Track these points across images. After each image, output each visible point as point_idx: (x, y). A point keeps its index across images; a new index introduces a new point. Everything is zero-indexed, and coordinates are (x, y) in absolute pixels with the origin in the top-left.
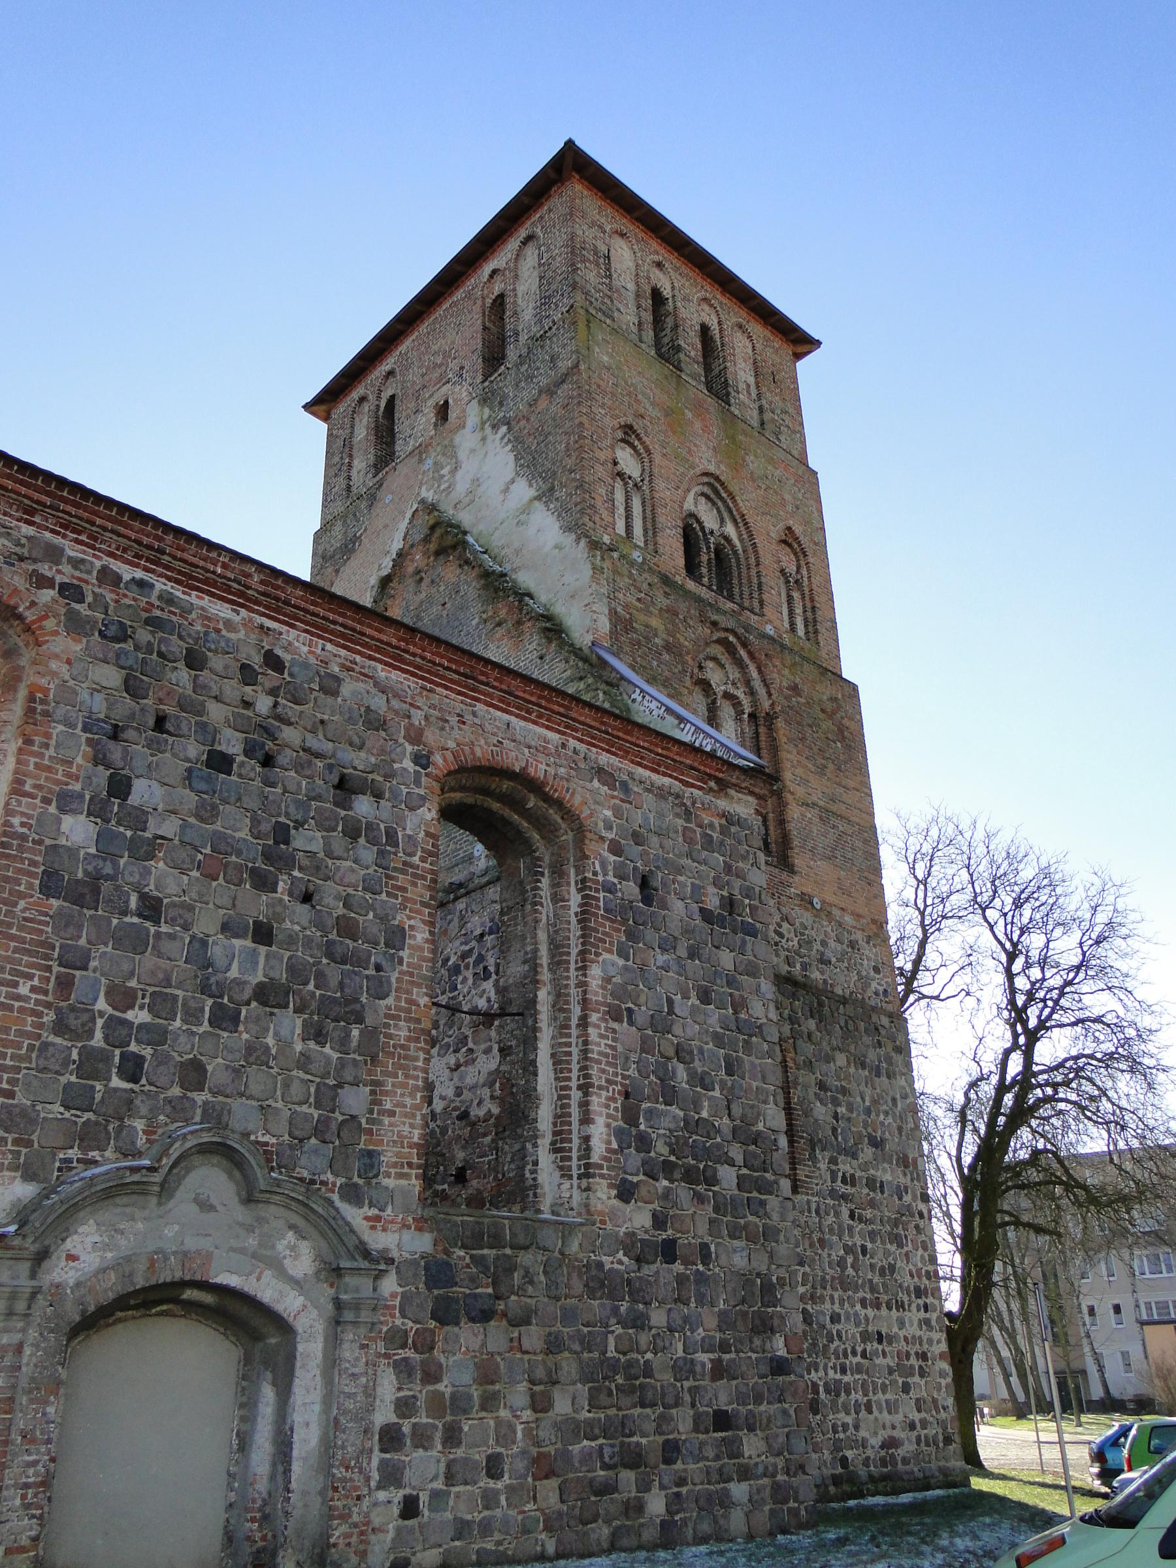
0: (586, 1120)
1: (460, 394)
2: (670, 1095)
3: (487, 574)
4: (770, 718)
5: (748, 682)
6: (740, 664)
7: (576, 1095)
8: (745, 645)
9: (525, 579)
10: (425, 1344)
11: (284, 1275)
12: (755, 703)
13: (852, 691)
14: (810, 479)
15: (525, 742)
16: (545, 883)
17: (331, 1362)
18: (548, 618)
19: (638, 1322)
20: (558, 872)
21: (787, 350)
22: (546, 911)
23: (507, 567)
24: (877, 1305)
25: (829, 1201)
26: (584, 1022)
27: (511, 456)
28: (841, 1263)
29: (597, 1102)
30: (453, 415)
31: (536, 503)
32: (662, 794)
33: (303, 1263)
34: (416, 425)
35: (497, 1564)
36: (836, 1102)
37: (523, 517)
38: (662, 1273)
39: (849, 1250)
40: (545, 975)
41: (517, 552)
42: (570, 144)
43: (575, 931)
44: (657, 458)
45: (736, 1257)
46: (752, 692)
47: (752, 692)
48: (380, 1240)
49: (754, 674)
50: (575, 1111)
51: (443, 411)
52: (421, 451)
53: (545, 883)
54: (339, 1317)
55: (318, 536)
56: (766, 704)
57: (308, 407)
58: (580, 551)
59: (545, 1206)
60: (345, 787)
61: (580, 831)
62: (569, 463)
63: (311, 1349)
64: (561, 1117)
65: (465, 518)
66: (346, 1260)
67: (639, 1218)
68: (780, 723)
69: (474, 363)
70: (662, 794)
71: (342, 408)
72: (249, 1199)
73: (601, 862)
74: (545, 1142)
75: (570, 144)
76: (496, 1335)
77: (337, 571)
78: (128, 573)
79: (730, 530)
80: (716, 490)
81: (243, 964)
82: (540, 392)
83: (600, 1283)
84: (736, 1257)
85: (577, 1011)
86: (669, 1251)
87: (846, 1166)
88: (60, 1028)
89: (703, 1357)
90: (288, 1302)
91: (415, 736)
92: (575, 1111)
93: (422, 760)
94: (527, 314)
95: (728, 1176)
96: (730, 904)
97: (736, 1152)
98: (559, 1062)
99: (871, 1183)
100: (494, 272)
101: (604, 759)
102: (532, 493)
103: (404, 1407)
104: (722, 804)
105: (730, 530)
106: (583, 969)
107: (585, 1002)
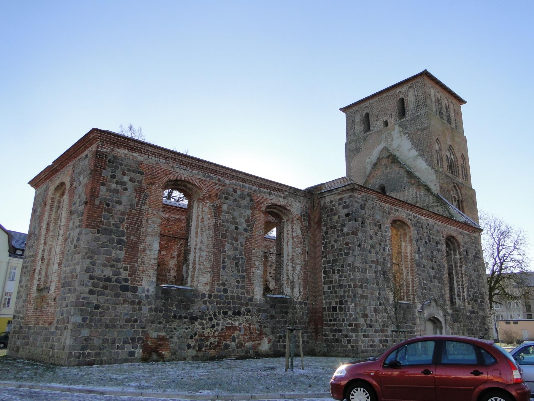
0: (463, 292)
2: (472, 288)
3: (408, 172)
4: (462, 202)
5: (457, 194)
6: (457, 190)
7: (461, 288)
8: (458, 186)
9: (417, 174)
10: (452, 325)
12: (459, 198)
14: (465, 139)
16: (452, 252)
17: (446, 327)
18: (426, 186)
19: (471, 323)
20: (455, 251)
21: (458, 103)
22: (453, 257)
23: (412, 170)
26: (462, 277)
27: (410, 143)
29: (465, 289)
30: (389, 125)
31: (419, 157)
32: (467, 235)
33: (442, 315)
34: (377, 125)
37: (415, 159)
38: (473, 315)
40: (454, 268)
41: (415, 167)
42: (426, 70)
43: (459, 261)
44: (442, 145)
46: (458, 196)
47: (458, 196)
49: (459, 191)
50: (461, 291)
51: (386, 123)
52: (380, 132)
53: (452, 252)
55: (346, 144)
56: (461, 198)
57: (340, 109)
58: (433, 171)
59: (457, 305)
61: (459, 244)
62: (428, 150)
64: (459, 291)
65: (397, 154)
67: (470, 308)
68: (464, 203)
69: (396, 113)
71: (350, 111)
72: (437, 306)
74: (456, 295)
75: (426, 70)
77: (355, 155)
78: (415, 215)
80: (450, 148)
82: (418, 129)
83: (468, 317)
85: (460, 275)
86: (474, 312)
89: (478, 328)
91: (442, 233)
92: (461, 291)
93: (443, 237)
94: (411, 107)
95: (479, 300)
98: (458, 283)
100: (400, 92)
101: (461, 230)
102: (417, 153)
104: (474, 235)
105: (452, 156)
106: (461, 268)
107: (462, 273)
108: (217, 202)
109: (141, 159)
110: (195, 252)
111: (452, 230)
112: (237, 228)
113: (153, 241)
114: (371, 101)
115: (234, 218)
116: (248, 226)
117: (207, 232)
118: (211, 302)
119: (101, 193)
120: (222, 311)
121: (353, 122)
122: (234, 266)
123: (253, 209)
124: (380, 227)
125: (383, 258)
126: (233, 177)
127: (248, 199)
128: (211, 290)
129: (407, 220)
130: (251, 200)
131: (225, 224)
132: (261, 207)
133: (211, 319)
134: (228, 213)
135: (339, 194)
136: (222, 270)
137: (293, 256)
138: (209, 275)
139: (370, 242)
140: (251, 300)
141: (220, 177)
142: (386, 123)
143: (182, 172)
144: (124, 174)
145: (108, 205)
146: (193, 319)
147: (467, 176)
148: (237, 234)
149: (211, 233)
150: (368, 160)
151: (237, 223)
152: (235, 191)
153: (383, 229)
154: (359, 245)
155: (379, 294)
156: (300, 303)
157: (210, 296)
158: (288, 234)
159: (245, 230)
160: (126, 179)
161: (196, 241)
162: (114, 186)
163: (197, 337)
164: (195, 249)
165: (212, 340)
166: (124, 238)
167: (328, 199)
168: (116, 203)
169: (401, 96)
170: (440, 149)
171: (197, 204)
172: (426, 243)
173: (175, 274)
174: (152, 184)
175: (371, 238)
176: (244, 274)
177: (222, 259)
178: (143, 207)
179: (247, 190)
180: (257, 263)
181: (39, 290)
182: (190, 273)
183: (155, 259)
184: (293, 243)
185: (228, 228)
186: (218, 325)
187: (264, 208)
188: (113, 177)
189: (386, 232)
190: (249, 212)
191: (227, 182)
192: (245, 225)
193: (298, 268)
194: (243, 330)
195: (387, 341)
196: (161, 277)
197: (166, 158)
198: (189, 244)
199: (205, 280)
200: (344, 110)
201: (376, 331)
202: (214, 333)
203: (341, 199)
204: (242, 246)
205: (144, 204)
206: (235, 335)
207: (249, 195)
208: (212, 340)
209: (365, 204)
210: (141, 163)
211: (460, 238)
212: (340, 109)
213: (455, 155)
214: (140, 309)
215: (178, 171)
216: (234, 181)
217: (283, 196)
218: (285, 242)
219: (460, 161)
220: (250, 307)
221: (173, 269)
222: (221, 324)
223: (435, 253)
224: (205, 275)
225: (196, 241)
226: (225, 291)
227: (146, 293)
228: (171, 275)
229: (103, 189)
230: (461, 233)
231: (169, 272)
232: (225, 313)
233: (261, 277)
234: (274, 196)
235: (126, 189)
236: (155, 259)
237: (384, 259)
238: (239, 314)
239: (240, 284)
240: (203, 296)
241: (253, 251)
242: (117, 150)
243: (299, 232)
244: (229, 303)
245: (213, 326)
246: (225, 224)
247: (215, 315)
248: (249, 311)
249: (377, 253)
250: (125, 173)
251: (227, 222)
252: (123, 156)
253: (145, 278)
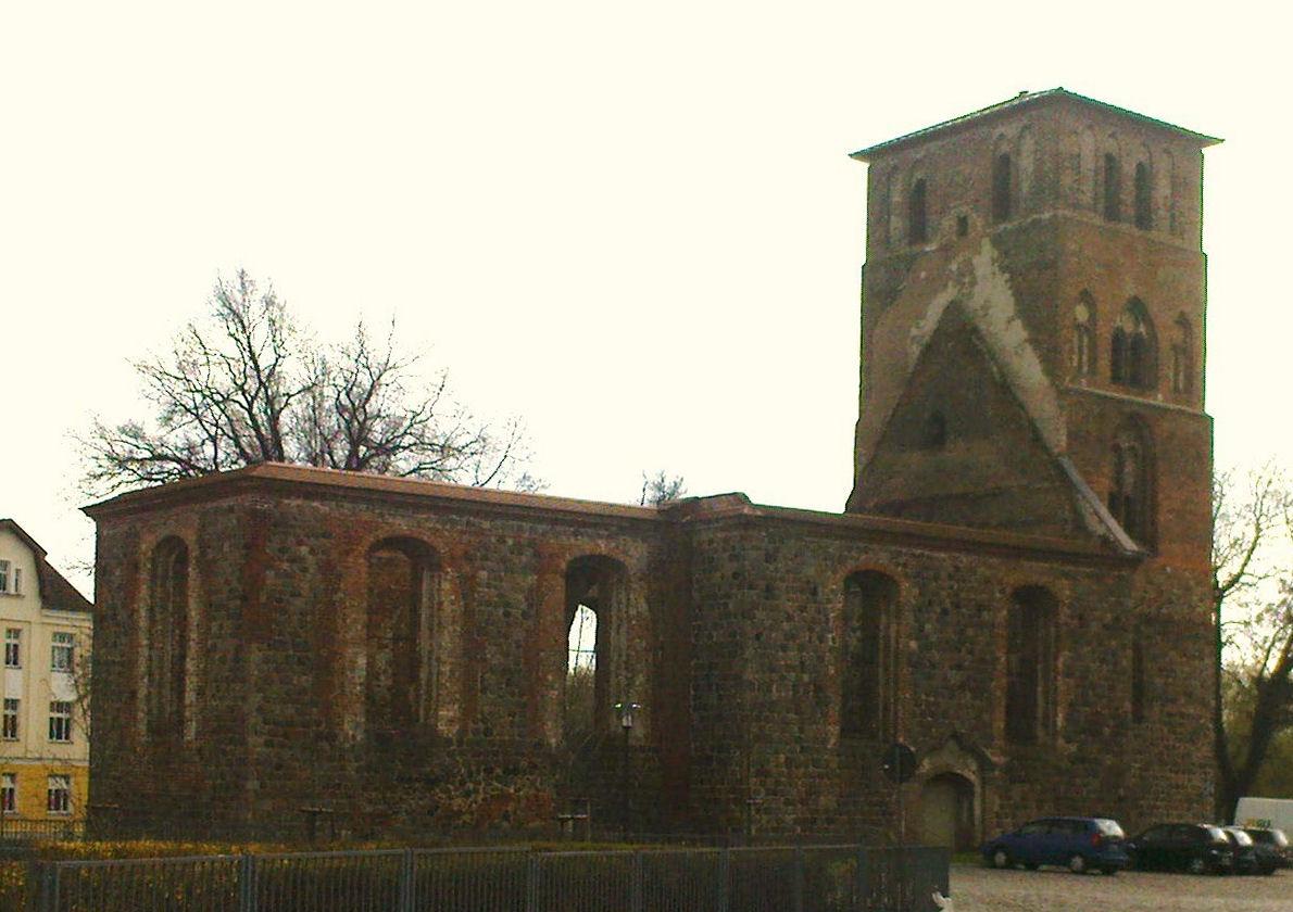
1: (977, 222)
11: (970, 772)
13: (1208, 422)
15: (1033, 572)
17: (983, 794)
24: (1177, 773)
25: (1158, 726)
28: (1161, 753)
32: (1088, 576)
33: (974, 767)
35: (1161, 908)
36: (1168, 677)
39: (1167, 747)
45: (1109, 760)
48: (995, 759)
54: (984, 782)
60: (980, 608)
63: (978, 789)
66: (984, 765)
70: (1088, 576)
73: (1064, 614)
76: (1027, 787)
79: (1142, 329)
81: (955, 677)
84: (1109, 760)
86: (1083, 760)
87: (1169, 708)
88: (916, 705)
90: (973, 778)
93: (1002, 591)
96: (1117, 619)
97: (1111, 723)
99: (1182, 715)
103: (1002, 807)
105: (1142, 329)
108: (467, 569)
109: (325, 509)
110: (430, 665)
111: (1033, 572)
112: (507, 614)
113: (356, 654)
114: (933, 146)
115: (501, 596)
116: (531, 606)
117: (451, 628)
118: (462, 753)
119: (268, 582)
120: (483, 767)
121: (886, 199)
122: (504, 686)
123: (540, 571)
124: (814, 592)
125: (819, 657)
126: (498, 515)
127: (529, 552)
128: (463, 731)
129: (893, 567)
130: (537, 554)
131: (483, 608)
132: (558, 566)
133: (463, 783)
134: (489, 586)
135: (722, 529)
136: (479, 694)
137: (628, 655)
138: (456, 706)
139: (786, 626)
140: (539, 745)
141: (472, 518)
142: (963, 222)
143: (399, 521)
144: (300, 543)
145: (280, 601)
146: (431, 782)
147: (1191, 382)
148: (508, 624)
149: (459, 629)
150: (914, 331)
151: (508, 604)
152: (502, 540)
153: (820, 596)
154: (758, 637)
155: (801, 730)
156: (642, 749)
157: (460, 743)
158: (619, 610)
159: (525, 615)
160: (304, 550)
161: (431, 645)
162: (285, 566)
163: (439, 811)
164: (430, 659)
165: (467, 818)
166: (310, 655)
167: (705, 537)
168: (292, 596)
169: (1005, 148)
170: (1093, 318)
171: (429, 574)
172: (945, 612)
173: (390, 682)
174: (347, 553)
175: (789, 618)
176: (525, 699)
177: (480, 674)
178: (335, 598)
179: (526, 535)
180: (550, 677)
181: (154, 730)
182: (422, 703)
183: (361, 684)
184: (631, 628)
185: (490, 614)
186: (476, 791)
187: (563, 566)
188: (282, 550)
189: (829, 601)
190: (532, 579)
191: (486, 525)
192: (524, 606)
193: (640, 679)
194: (524, 802)
195: (814, 821)
196: (373, 713)
197: (369, 501)
198: (418, 649)
199: (451, 714)
200: (859, 155)
201: (787, 803)
202: (470, 806)
203: (726, 540)
204: (518, 647)
205: (335, 591)
206: (509, 808)
207: (532, 543)
208: (467, 818)
209: (777, 550)
210: (326, 517)
211: (1064, 590)
212: (851, 155)
213: (1150, 324)
214: (343, 768)
215: (391, 520)
216: (499, 522)
217: (606, 533)
218: (614, 626)
219: (1168, 335)
220: (538, 761)
221: (385, 672)
222: (481, 791)
223: (970, 632)
224: (450, 707)
225: (431, 645)
226: (488, 732)
227: (352, 742)
228: (382, 684)
229: (270, 574)
230: (1066, 575)
231: (377, 679)
232: (489, 771)
233: (996, 334)
234: (586, 539)
235: (305, 570)
236: (361, 684)
237: (821, 659)
238: (515, 771)
239: (517, 719)
240: (449, 741)
241: (542, 654)
242: (286, 501)
243: (643, 607)
244: (496, 754)
245: (467, 794)
246: (483, 608)
247: (470, 774)
248: (535, 767)
249: (801, 648)
250: (302, 540)
251: (489, 604)
252: (295, 510)
253: (348, 718)
